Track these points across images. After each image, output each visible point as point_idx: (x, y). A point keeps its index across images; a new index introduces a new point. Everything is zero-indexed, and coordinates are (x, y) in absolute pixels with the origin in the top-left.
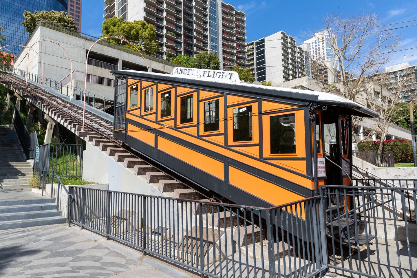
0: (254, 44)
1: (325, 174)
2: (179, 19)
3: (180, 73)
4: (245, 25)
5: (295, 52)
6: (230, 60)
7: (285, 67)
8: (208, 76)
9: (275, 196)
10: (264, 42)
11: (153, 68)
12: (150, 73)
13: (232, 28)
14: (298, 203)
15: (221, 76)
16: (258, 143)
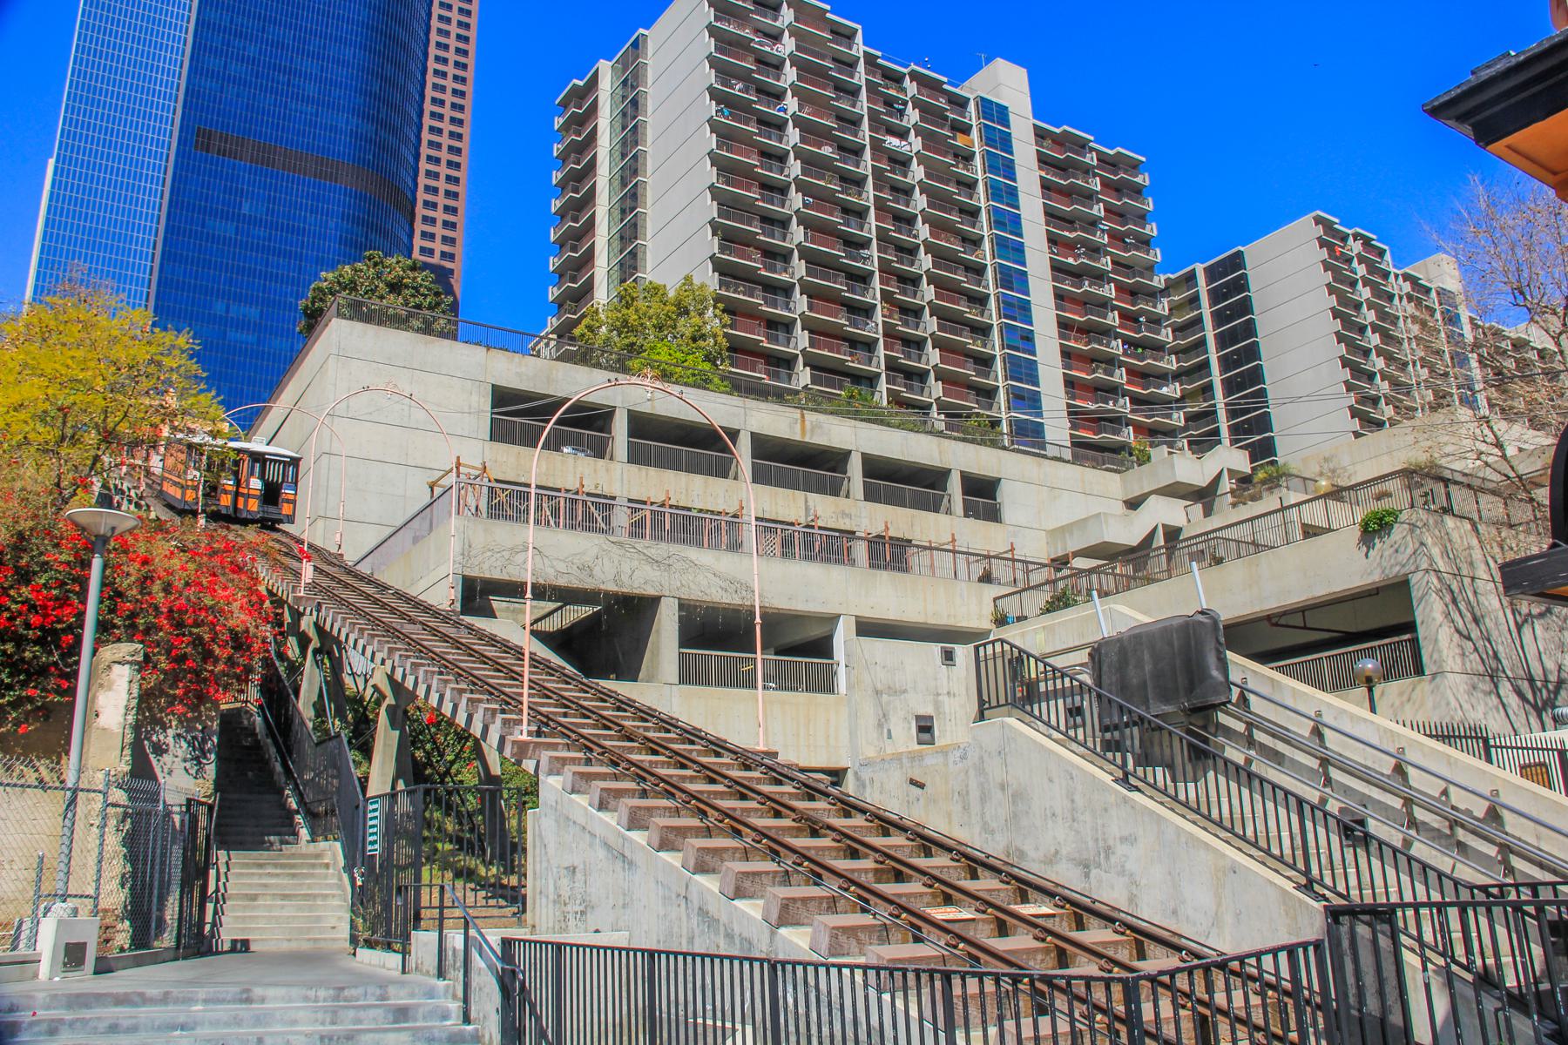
2: (855, 244)
5: (1390, 297)
6: (1091, 359)
10: (1242, 266)
13: (1093, 223)
14: (1266, 952)
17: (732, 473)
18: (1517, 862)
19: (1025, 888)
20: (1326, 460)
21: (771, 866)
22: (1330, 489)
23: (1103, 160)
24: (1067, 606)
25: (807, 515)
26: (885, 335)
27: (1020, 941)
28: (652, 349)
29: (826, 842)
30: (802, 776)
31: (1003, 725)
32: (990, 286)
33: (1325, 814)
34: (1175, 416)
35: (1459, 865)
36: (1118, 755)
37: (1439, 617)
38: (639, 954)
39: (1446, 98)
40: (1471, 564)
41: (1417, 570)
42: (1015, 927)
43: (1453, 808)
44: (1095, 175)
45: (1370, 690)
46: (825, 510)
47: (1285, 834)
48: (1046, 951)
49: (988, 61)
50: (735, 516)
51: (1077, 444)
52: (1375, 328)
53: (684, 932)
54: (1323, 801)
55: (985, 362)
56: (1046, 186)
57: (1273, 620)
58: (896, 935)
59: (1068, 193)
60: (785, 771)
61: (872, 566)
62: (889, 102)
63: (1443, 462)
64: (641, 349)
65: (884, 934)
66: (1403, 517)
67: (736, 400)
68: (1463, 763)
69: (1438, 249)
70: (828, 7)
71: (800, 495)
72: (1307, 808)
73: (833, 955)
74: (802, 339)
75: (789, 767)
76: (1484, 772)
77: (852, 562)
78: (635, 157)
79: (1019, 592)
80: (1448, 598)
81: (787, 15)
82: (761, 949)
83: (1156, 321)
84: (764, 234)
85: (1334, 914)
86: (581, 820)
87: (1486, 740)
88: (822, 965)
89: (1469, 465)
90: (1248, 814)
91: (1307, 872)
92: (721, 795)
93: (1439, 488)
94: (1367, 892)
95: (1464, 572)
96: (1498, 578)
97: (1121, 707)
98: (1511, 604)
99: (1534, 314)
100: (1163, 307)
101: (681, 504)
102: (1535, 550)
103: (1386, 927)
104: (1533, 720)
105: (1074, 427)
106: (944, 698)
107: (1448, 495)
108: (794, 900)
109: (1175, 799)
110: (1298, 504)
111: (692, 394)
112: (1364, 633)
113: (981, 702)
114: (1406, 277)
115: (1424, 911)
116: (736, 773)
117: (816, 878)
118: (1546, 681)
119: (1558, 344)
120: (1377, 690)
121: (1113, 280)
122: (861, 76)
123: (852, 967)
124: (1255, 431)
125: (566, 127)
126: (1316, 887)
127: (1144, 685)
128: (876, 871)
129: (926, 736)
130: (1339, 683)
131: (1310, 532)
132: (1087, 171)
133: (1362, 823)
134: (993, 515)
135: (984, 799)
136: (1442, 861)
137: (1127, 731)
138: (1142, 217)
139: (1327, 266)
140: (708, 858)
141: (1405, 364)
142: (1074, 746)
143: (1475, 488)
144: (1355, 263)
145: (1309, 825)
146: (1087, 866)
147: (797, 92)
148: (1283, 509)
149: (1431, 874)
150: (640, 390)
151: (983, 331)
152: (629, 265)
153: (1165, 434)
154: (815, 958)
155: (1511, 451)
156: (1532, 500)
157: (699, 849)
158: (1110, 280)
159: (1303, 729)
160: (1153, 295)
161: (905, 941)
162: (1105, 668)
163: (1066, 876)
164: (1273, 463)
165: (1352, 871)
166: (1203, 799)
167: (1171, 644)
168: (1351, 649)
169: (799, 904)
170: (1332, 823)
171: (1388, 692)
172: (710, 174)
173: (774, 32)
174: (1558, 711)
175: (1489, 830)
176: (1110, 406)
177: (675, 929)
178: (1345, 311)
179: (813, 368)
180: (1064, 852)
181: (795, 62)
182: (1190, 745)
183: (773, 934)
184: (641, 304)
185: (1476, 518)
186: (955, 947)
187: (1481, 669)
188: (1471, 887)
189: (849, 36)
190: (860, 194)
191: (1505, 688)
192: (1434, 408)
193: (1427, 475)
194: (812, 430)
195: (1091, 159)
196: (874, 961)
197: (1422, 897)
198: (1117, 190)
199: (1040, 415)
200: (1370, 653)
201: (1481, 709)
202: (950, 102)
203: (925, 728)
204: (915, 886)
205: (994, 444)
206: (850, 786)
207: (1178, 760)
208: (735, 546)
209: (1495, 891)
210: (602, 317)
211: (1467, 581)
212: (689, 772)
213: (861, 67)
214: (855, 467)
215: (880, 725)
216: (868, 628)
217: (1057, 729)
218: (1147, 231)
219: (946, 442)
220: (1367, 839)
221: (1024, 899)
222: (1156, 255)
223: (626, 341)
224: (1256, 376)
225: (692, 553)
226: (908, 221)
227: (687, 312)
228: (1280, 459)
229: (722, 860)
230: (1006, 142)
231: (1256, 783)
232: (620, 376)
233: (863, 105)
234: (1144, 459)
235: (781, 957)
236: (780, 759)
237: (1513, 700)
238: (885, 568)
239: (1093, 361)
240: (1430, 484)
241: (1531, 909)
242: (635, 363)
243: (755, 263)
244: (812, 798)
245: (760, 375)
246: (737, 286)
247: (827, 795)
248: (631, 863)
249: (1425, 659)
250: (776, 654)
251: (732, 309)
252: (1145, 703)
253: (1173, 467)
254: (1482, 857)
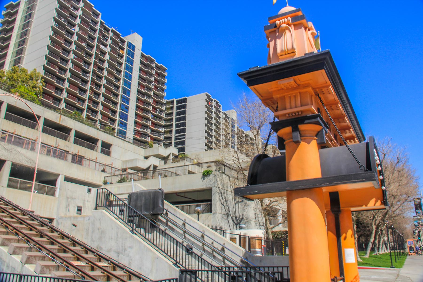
0: (175, 103)
4: (166, 81)
5: (220, 118)
6: (143, 118)
7: (209, 122)
11: (46, 117)
13: (150, 82)
17: (36, 128)
18: (226, 261)
19: (101, 258)
20: (197, 155)
21: (27, 245)
22: (197, 163)
23: (157, 66)
24: (124, 182)
25: (56, 144)
26: (89, 99)
27: (97, 273)
28: (19, 87)
29: (45, 239)
30: (41, 219)
31: (102, 212)
32: (120, 92)
33: (183, 245)
34: (161, 137)
35: (213, 261)
36: (132, 224)
37: (218, 199)
39: (243, 73)
40: (227, 187)
41: (214, 186)
42: (96, 269)
43: (214, 247)
44: (154, 70)
45: (198, 215)
46: (62, 144)
47: (172, 250)
48: (104, 276)
49: (133, 33)
50: (35, 141)
51: (135, 139)
52: (215, 125)
54: (183, 242)
55: (114, 112)
56: (141, 69)
57: (177, 194)
58: (61, 269)
59: (146, 73)
60: (36, 217)
61: (72, 162)
62: (104, 36)
63: (225, 161)
64: (16, 86)
65: (58, 268)
66: (213, 173)
67: (42, 108)
68: (218, 235)
69: (233, 108)
70: (94, 6)
71: (55, 138)
72: (178, 244)
73: (41, 273)
74: (65, 95)
75: (37, 216)
76: (222, 239)
77: (66, 160)
78: (27, 31)
79: (112, 176)
80: (220, 195)
81: (81, 4)
82: (18, 271)
83: (161, 111)
84: (60, 63)
85: (182, 272)
87: (224, 231)
88: (37, 276)
89: (231, 163)
90: (163, 244)
91: (176, 261)
92: (14, 222)
93: (223, 167)
94: (190, 267)
95: (225, 189)
96: (233, 191)
97: (134, 211)
98: (235, 198)
99: (251, 129)
100: (164, 108)
101: (19, 134)
102: (242, 186)
103: (194, 276)
104: (235, 227)
105: (135, 134)
106: (86, 202)
107: (225, 169)
108: (32, 256)
109: (145, 238)
110: (188, 165)
111: (29, 103)
112: (199, 200)
113: (97, 204)
114: (225, 114)
115: (203, 272)
116: (20, 216)
117: (40, 250)
118: (239, 218)
119: (255, 137)
120: (200, 215)
121: (153, 98)
122: (98, 27)
123: (46, 278)
124: (181, 145)
125: (6, 15)
126: (178, 264)
127: (141, 206)
128: (58, 249)
129: (79, 212)
130: (191, 213)
131: (190, 173)
132: (152, 68)
133: (191, 249)
134: (108, 154)
135: (93, 232)
136: (209, 260)
137: (135, 218)
138: (163, 84)
139: (206, 107)
141: (220, 135)
142: (120, 220)
143: (231, 169)
144: (213, 107)
145: (178, 248)
146: (119, 253)
147: (79, 26)
148: (184, 166)
149: (206, 263)
150: (13, 99)
151: (115, 104)
152: (17, 61)
153: (158, 141)
154: (35, 274)
155: (241, 161)
156: (243, 173)
158: (152, 98)
159: (180, 223)
160: (162, 104)
161: (64, 271)
162: (132, 200)
163: (113, 256)
164: (184, 154)
165: (187, 261)
166: (152, 238)
167: (150, 196)
168: (195, 204)
169: (33, 258)
170: (184, 248)
171: (203, 216)
172: (49, 42)
173: (77, 8)
174: (241, 225)
175: (221, 253)
176: (145, 130)
178: (209, 119)
179: (66, 103)
180: (113, 249)
181: (81, 17)
182: (151, 224)
183: (23, 266)
184: (19, 74)
185: (230, 176)
186: (78, 273)
187: (225, 213)
188: (215, 267)
189: (97, 15)
190: (90, 59)
191: (230, 219)
192: (225, 147)
193: (221, 163)
195: (154, 65)
196: (53, 276)
197: (203, 269)
198: (159, 75)
199: (126, 129)
200: (200, 206)
201: (224, 223)
202: (121, 41)
203: (79, 210)
204: (69, 255)
205: (112, 135)
206: (54, 224)
207: (147, 227)
208: (33, 149)
209: (220, 268)
210: (5, 74)
211: (225, 191)
212: (5, 214)
213: (99, 24)
214: (73, 134)
215: (67, 207)
216: (68, 179)
217: (116, 215)
218: (164, 87)
219: (99, 132)
220: (192, 253)
221: (100, 261)
222: (165, 94)
223: (12, 83)
224: (184, 130)
225: (19, 149)
226: (101, 69)
227: (32, 79)
228: (186, 153)
229: (10, 242)
230: (133, 55)
231: (167, 236)
232: (7, 93)
233: (97, 35)
234: (151, 146)
235: (24, 273)
236: (35, 214)
237: (231, 222)
238: (76, 163)
239: (143, 118)
240: (221, 166)
241: (227, 273)
242: (13, 90)
243: (56, 70)
244: (42, 226)
245: (51, 102)
246: (49, 75)
247: (47, 225)
249: (213, 209)
250: (39, 182)
251: (46, 82)
252: (141, 211)
253: (158, 150)
254: (219, 260)
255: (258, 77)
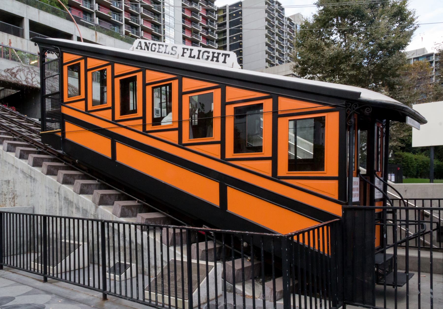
1: (358, 198)
3: (145, 49)
5: (283, 25)
8: (190, 56)
9: (283, 223)
12: (74, 42)
15: (210, 58)
16: (270, 155)
26: (125, 11)
38: (39, 217)
53: (58, 206)
86: (12, 162)
140: (68, 178)
157: (64, 175)
177: (54, 205)
183: (96, 208)
194: (100, 39)
229: (74, 179)
248: (34, 179)
255: (48, 260)
